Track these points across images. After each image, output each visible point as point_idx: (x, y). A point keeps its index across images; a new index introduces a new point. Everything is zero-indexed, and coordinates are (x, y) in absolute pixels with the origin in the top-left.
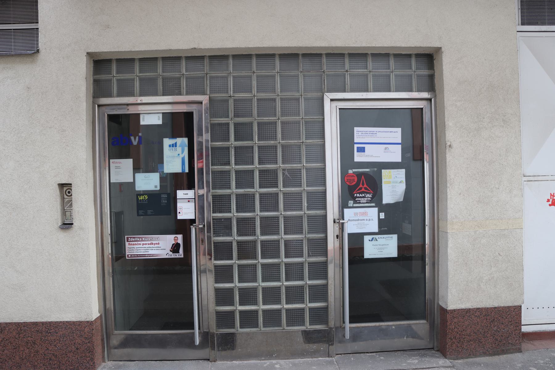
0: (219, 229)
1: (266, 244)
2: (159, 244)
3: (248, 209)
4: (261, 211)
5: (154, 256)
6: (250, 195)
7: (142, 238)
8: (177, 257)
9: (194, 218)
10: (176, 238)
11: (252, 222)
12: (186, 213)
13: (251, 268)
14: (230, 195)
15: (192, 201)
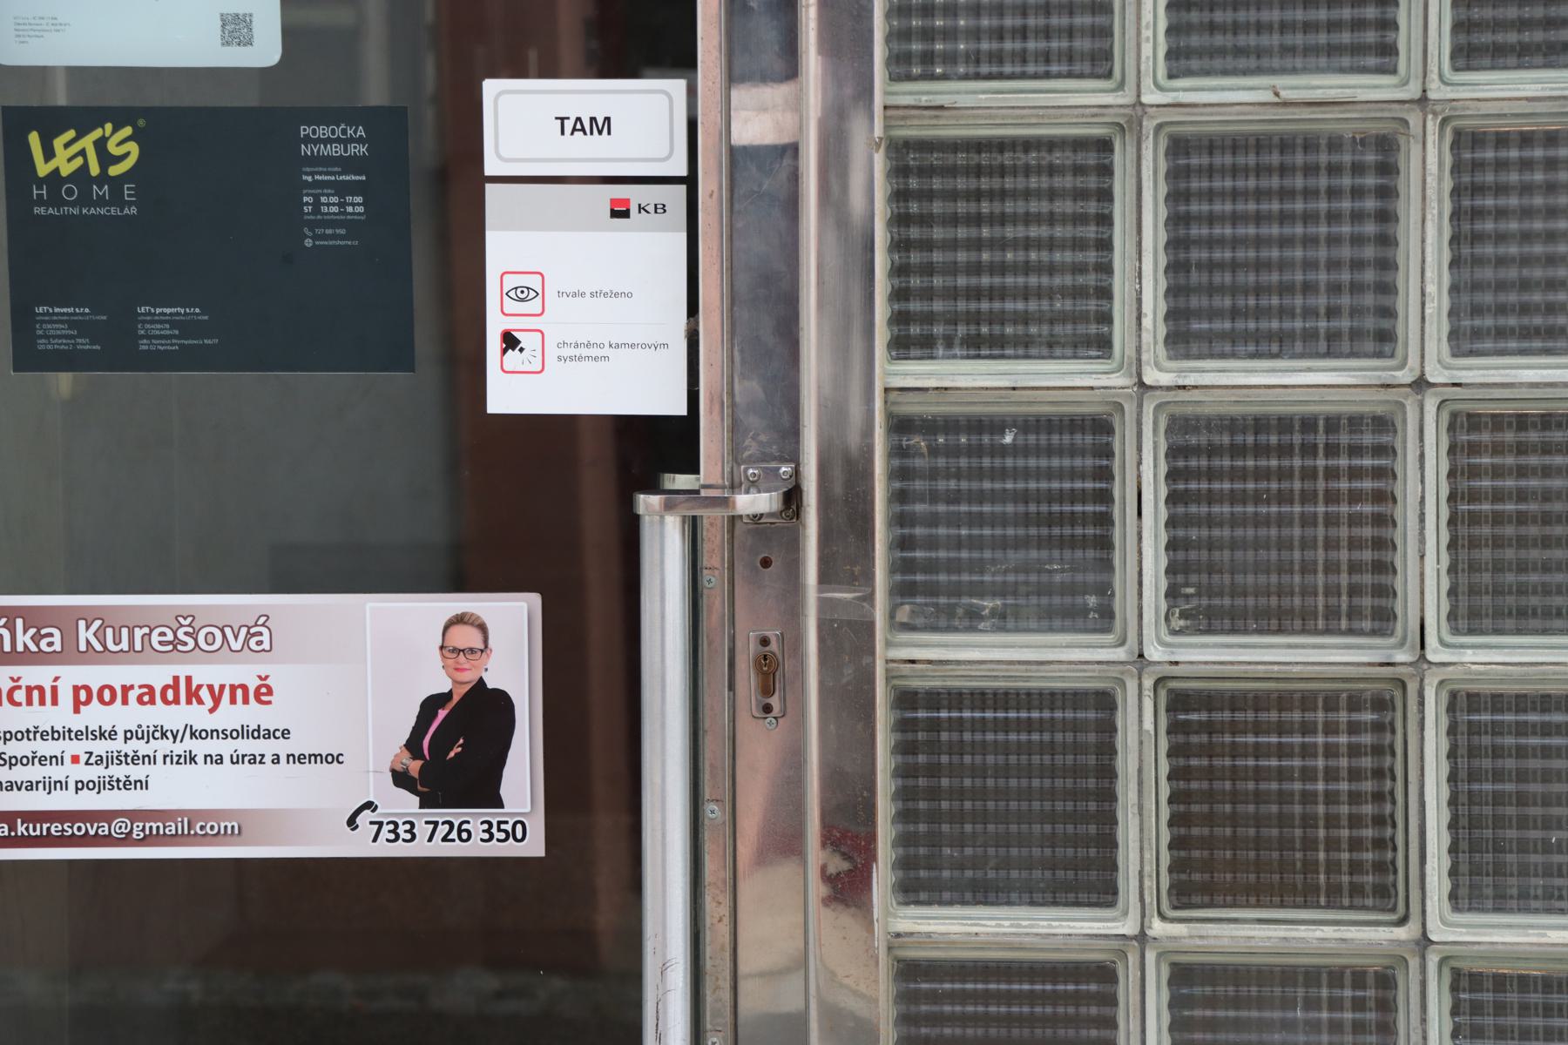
0: (958, 544)
1: (1521, 729)
2: (263, 693)
3: (1310, 313)
4: (1464, 341)
5: (204, 839)
6: (1335, 144)
7: (67, 621)
8: (475, 848)
9: (681, 409)
10: (466, 637)
11: (1355, 473)
12: (584, 352)
13: (1335, 1004)
14: (1105, 145)
15: (660, 209)
